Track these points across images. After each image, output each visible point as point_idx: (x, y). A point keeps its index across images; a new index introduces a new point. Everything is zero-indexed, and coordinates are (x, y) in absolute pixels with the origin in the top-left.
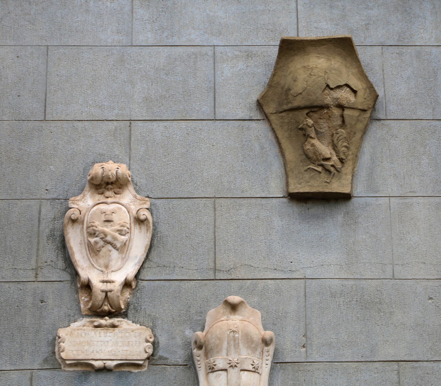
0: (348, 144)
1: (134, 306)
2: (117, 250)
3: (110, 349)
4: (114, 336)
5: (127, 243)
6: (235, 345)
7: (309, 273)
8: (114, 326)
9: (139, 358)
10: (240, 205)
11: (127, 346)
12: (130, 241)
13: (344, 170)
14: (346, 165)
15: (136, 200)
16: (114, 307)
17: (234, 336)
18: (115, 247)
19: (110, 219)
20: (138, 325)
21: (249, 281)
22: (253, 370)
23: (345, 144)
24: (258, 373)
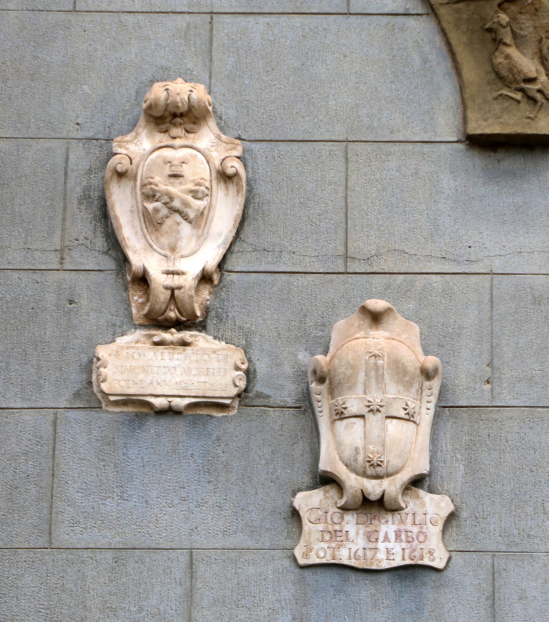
2: (190, 222)
3: (178, 379)
5: (206, 212)
6: (377, 378)
7: (498, 265)
8: (184, 344)
12: (209, 208)
16: (184, 314)
17: (376, 364)
18: (186, 218)
22: (407, 417)
24: (415, 422)
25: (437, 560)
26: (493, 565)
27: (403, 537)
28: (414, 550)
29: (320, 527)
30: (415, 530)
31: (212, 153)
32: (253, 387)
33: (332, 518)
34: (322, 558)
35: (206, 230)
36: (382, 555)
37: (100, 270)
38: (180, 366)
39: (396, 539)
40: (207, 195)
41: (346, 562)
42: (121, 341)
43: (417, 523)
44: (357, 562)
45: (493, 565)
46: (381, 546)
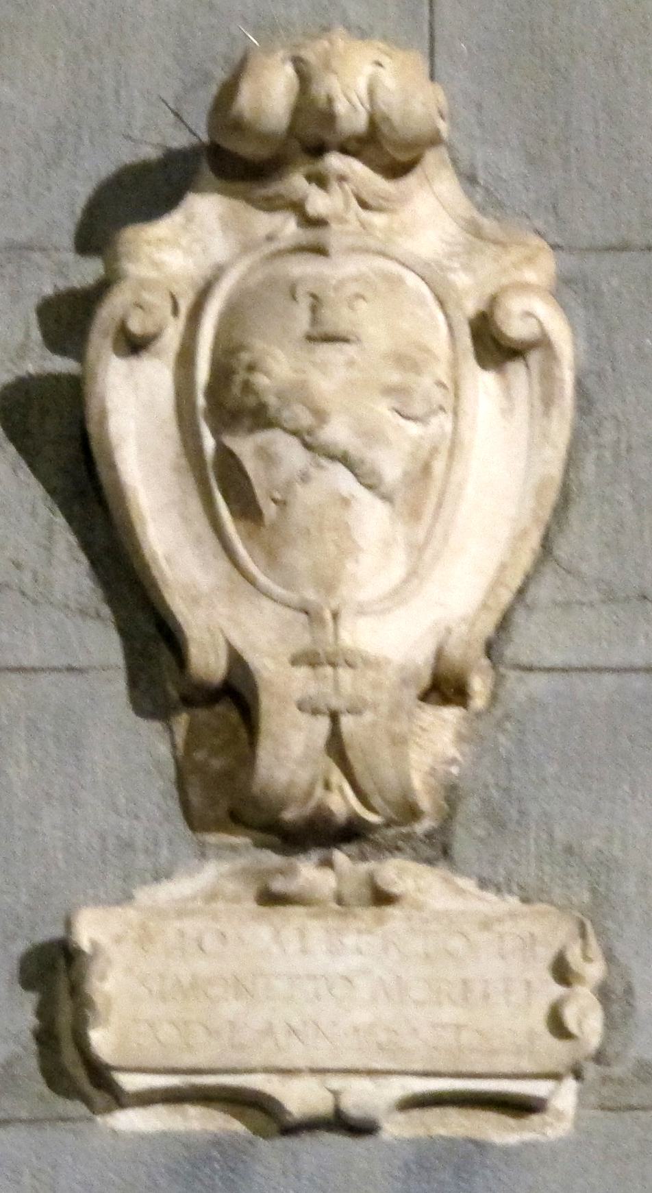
1: (486, 801)
2: (387, 498)
3: (362, 1017)
4: (385, 950)
5: (439, 466)
8: (382, 898)
9: (527, 1066)
10: (518, 1052)
11: (454, 1003)
12: (451, 454)
15: (479, 243)
16: (376, 801)
32: (625, 1045)
37: (70, 669)
38: (366, 972)
40: (442, 408)
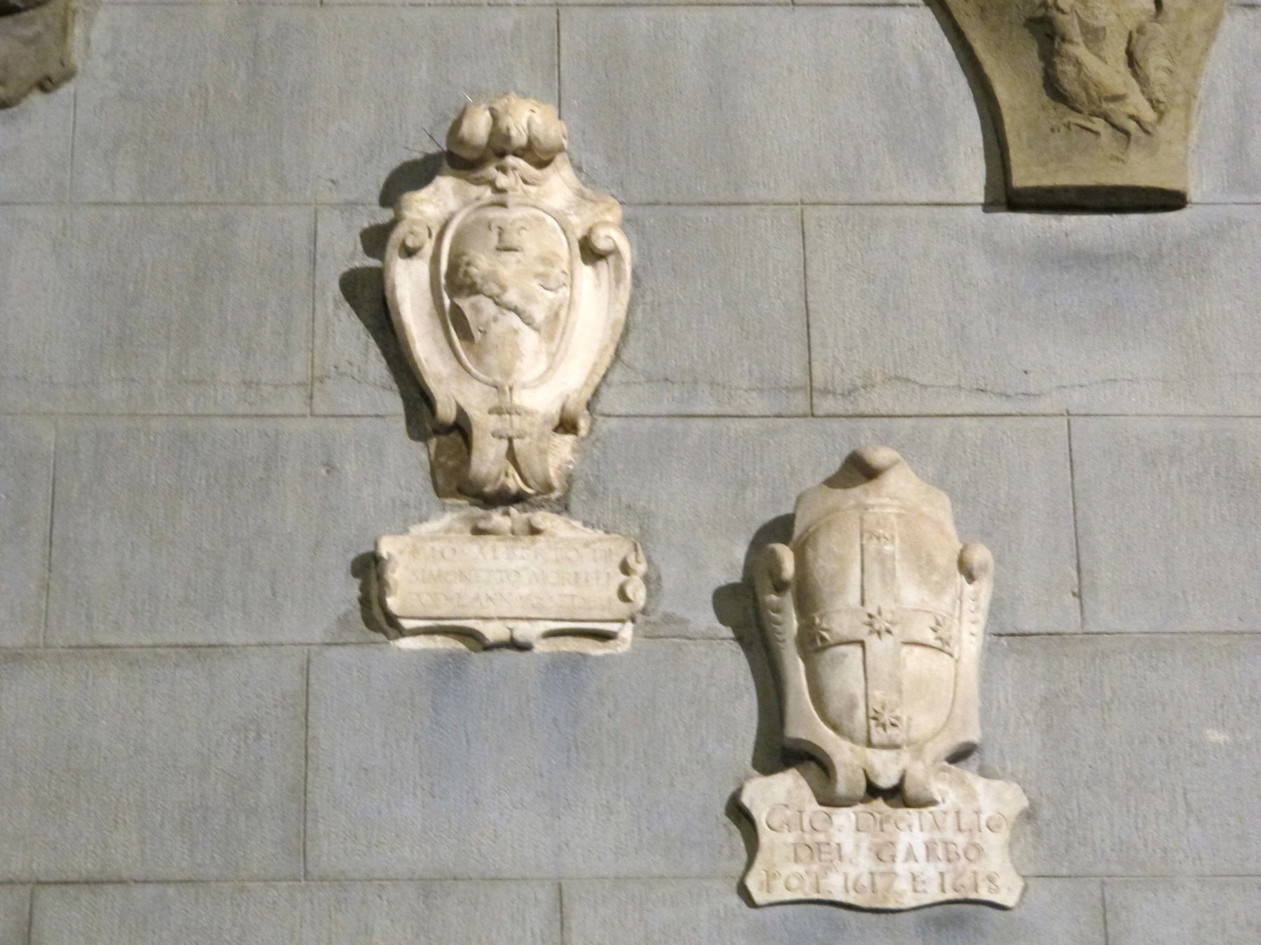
0: (1172, 61)
1: (587, 482)
2: (537, 330)
3: (524, 591)
5: (563, 314)
6: (883, 576)
7: (1076, 400)
8: (534, 531)
9: (607, 616)
12: (569, 308)
13: (1162, 131)
14: (1169, 119)
16: (532, 482)
17: (880, 552)
18: (528, 321)
19: (552, 639)
20: (600, 533)
21: (909, 422)
22: (938, 644)
23: (1166, 63)
24: (951, 655)
25: (1004, 891)
26: (1103, 900)
27: (940, 852)
28: (961, 875)
29: (790, 837)
30: (961, 840)
31: (570, 218)
33: (811, 822)
34: (795, 890)
35: (563, 346)
36: (903, 885)
39: (928, 856)
41: (839, 896)
42: (416, 530)
43: (963, 827)
44: (859, 897)
45: (1103, 900)
46: (901, 867)
